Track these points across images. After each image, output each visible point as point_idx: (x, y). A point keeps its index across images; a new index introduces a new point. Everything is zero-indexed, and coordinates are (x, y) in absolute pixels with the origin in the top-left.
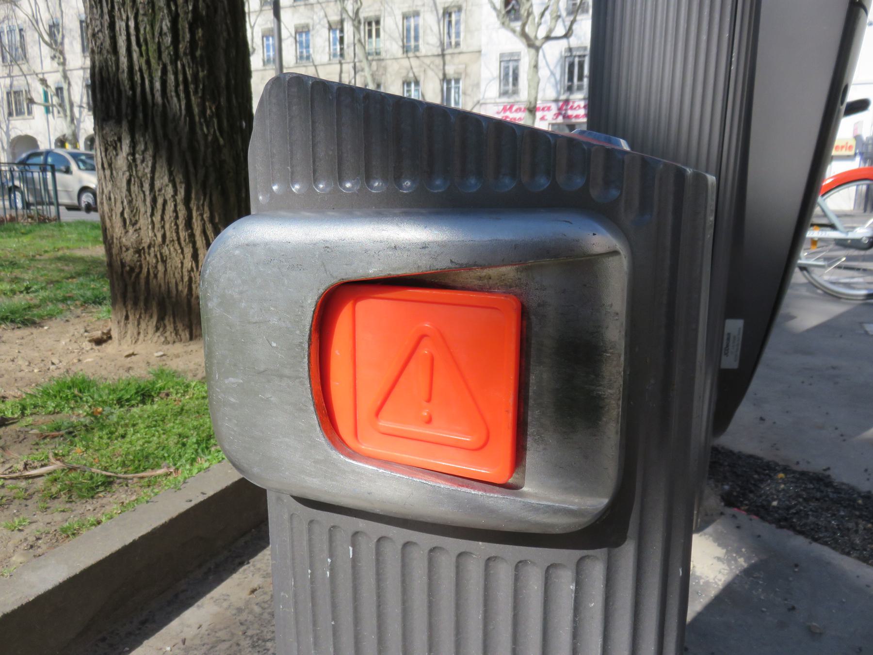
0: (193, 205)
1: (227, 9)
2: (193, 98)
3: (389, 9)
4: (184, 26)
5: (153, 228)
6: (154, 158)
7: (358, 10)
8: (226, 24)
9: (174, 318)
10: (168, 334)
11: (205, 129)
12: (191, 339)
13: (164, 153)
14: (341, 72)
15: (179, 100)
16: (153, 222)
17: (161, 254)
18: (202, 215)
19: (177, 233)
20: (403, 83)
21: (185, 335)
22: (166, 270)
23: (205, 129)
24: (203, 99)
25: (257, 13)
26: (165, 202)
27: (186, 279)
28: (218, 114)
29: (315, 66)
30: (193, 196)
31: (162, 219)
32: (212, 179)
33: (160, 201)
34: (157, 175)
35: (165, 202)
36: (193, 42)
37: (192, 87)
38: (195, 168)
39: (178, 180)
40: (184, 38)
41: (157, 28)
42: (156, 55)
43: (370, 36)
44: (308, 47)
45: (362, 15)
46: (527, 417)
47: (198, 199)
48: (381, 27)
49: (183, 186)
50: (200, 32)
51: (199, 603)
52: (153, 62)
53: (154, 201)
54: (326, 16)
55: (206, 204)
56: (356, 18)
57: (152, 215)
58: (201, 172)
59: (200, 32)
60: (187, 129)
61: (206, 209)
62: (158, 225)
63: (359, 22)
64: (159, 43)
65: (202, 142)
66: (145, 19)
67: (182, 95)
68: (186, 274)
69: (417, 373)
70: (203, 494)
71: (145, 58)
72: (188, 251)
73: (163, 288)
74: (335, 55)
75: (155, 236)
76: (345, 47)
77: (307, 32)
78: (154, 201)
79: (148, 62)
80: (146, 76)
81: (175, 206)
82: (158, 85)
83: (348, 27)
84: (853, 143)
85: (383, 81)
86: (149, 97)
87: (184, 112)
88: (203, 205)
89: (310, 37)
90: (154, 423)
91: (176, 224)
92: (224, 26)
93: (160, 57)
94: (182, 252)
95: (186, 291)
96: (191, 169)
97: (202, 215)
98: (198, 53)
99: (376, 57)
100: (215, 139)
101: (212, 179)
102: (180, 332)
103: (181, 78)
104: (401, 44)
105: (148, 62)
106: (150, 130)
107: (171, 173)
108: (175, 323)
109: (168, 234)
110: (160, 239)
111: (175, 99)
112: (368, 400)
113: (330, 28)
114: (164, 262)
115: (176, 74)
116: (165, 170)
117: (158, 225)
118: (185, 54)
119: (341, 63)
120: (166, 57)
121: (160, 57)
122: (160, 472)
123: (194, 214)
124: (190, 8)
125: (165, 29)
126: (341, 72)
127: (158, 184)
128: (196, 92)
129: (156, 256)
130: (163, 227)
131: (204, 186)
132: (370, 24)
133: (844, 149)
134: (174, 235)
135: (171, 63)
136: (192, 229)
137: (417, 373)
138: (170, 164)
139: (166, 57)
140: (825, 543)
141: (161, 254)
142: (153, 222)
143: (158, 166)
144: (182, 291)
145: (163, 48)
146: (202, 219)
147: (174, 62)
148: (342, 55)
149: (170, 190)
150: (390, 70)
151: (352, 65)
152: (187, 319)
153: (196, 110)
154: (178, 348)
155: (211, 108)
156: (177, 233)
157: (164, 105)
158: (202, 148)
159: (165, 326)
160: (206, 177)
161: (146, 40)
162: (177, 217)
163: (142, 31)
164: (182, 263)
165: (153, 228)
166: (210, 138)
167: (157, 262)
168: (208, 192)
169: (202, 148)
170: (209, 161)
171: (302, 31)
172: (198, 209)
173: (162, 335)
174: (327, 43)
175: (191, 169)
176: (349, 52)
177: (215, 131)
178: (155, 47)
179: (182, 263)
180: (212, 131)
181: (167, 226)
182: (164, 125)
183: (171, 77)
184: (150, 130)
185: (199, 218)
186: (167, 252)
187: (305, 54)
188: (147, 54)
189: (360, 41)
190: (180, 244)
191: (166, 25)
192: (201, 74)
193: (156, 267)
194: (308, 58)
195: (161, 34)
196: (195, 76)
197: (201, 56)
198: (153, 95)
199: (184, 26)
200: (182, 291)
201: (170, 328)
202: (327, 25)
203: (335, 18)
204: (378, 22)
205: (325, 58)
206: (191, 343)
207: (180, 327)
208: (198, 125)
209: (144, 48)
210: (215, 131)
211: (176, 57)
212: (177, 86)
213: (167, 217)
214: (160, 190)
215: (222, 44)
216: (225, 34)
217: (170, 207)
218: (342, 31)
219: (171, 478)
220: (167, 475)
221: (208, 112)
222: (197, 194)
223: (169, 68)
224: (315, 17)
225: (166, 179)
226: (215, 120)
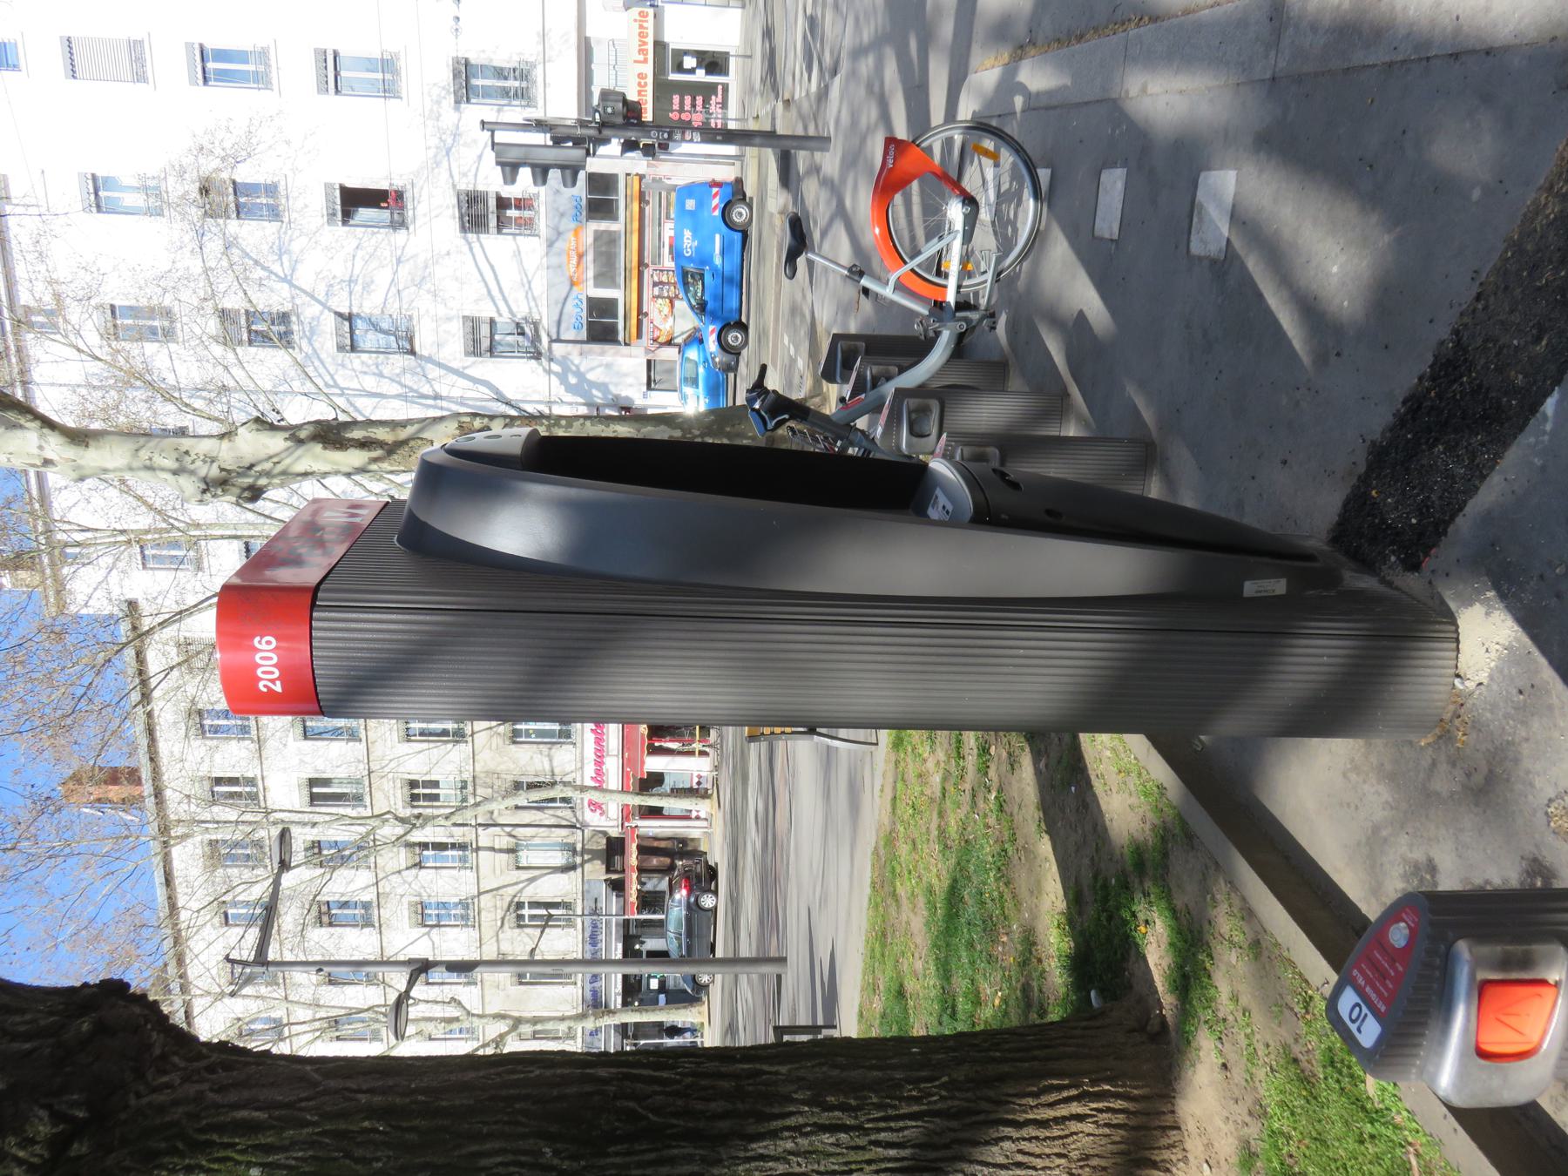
0: (1021, 1117)
1: (797, 1065)
2: (902, 1111)
3: (393, 765)
4: (826, 1118)
5: (1050, 1168)
6: (971, 1162)
7: (397, 818)
8: (813, 1067)
9: (1154, 1149)
10: (1174, 1158)
11: (935, 1098)
12: (1179, 1128)
13: (966, 1150)
14: (492, 849)
15: (907, 1128)
16: (1043, 1169)
17: (1079, 1160)
18: (1032, 1107)
19: (1054, 1138)
20: (514, 742)
21: (1174, 1135)
22: (1097, 1155)
23: (935, 1098)
24: (901, 1099)
25: (388, 989)
26: (1020, 1151)
27: (1107, 1131)
28: (915, 1082)
29: (480, 894)
30: (1010, 1117)
31: (1039, 1156)
32: (991, 1093)
33: (1020, 1158)
34: (990, 1160)
35: (1020, 1151)
36: (843, 1108)
37: (891, 1112)
38: (979, 1113)
39: (996, 1135)
40: (839, 1119)
41: (832, 1149)
42: (861, 1152)
43: (436, 797)
44: (444, 905)
45: (406, 812)
46: (1050, 478)
47: (1014, 1112)
48: (420, 778)
49: (1001, 1128)
50: (831, 1099)
51: (1561, 1125)
52: (867, 1156)
53: (1019, 1165)
54: (399, 872)
55: (1018, 1102)
56: (409, 823)
57: (1034, 1168)
58: (984, 1105)
59: (831, 1099)
60: (937, 1120)
61: (1024, 1101)
62: (1047, 1163)
63: (418, 817)
64: (847, 1148)
65: (950, 1103)
66: (823, 1162)
67: (901, 1124)
68: (1101, 1131)
69: (1511, 1020)
70: (1445, 1117)
71: (865, 1166)
72: (1074, 1126)
73: (1119, 1160)
74: (463, 859)
75: (1058, 1166)
76: (450, 840)
77: (423, 906)
78: (1019, 1165)
79: (869, 1162)
80: (883, 1166)
81: (1024, 1139)
82: (892, 1153)
83: (417, 836)
84: (635, 11)
85: (510, 778)
86: (905, 1164)
87: (919, 1123)
88: (1020, 1105)
89: (433, 900)
90: (1341, 1170)
91: (1045, 1139)
92: (817, 1069)
93: (863, 1148)
94: (1076, 1133)
95: (1121, 1132)
96: (981, 1117)
97: (1032, 1107)
98: (853, 1102)
99: (470, 788)
100: (943, 1086)
101: (991, 1093)
102: (1171, 1142)
103: (883, 1125)
104: (450, 746)
105: (869, 1162)
106: (942, 1165)
107: (987, 1143)
108: (1160, 1148)
109: (1056, 1150)
110: (1062, 1161)
111: (906, 1133)
112: (1517, 1037)
113: (419, 865)
114: (1087, 1157)
115: (879, 1130)
116: (983, 1149)
117: (1047, 1163)
118: (856, 1118)
119: (478, 849)
120: (862, 1141)
121: (863, 1148)
122: (1414, 1162)
123: (1031, 1116)
124: (806, 1109)
125: (832, 1140)
126: (492, 849)
127: (1001, 1160)
128: (894, 1107)
129: (1081, 1167)
130: (1048, 1156)
131: (999, 1103)
132: (414, 797)
133: (645, 24)
134: (1056, 1142)
135: (868, 1135)
136: (1048, 1121)
137: (1503, 1018)
138: (976, 1144)
139: (862, 1141)
140: (1465, 502)
141: (1079, 1160)
142: (1043, 1169)
143: (980, 1159)
144: (1122, 1137)
145: (852, 1144)
146: (1036, 1106)
147: (867, 1132)
148: (462, 847)
149: (1007, 1145)
150: (492, 766)
151: (480, 829)
152: (1155, 1133)
153: (915, 1108)
154: (1194, 1145)
155: (910, 1091)
156: (1054, 1138)
157: (913, 1146)
158: (956, 1103)
159: (1163, 1161)
160: (989, 1100)
161: (846, 1163)
162: (1037, 1138)
163: (836, 1167)
164: (1089, 1135)
165: (1050, 1168)
166: (944, 1093)
167: (1088, 1165)
168: (1004, 1098)
169: (956, 1103)
170: (969, 1095)
171: (426, 915)
172: (1026, 1112)
173: (1175, 1165)
174: (444, 872)
175: (981, 1117)
176: (459, 835)
177: (935, 1087)
178: (852, 1153)
179: (1089, 1135)
180: (935, 1090)
181: (1047, 1151)
182: (934, 1147)
183: (883, 1136)
184: (942, 1165)
185: (1035, 1111)
186: (1077, 1152)
187: (459, 911)
188: (860, 1162)
189: (447, 818)
190: (1066, 1136)
191: (828, 1138)
192: (875, 1100)
193: (1094, 1167)
194: (464, 904)
195: (837, 1145)
196: (879, 1107)
197: (855, 1099)
198: (903, 1159)
199: (826, 1118)
200: (1122, 1137)
201: (1166, 1155)
202: (414, 871)
203: (402, 857)
204: (413, 784)
205: (470, 875)
206: (1183, 1127)
207: (1164, 1141)
208: (931, 1107)
209: (853, 1167)
210: (935, 1087)
211: (859, 1128)
212: (891, 1129)
213: (1037, 1151)
214: (1007, 1157)
215: (835, 1073)
216: (825, 1069)
217: (1025, 1146)
218: (425, 846)
219: (1421, 1150)
220: (1418, 1155)
221: (914, 1093)
222: (1007, 1112)
223: (873, 1137)
224: (400, 891)
225: (995, 1149)
226: (922, 1086)
